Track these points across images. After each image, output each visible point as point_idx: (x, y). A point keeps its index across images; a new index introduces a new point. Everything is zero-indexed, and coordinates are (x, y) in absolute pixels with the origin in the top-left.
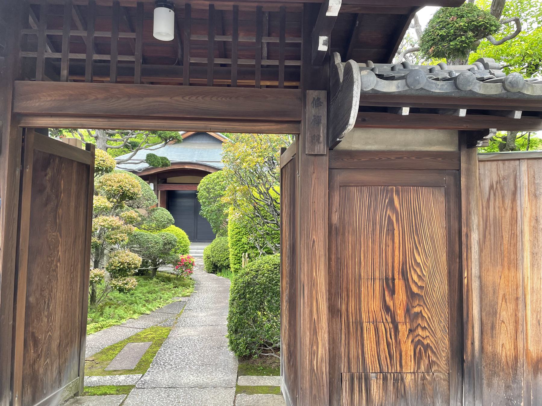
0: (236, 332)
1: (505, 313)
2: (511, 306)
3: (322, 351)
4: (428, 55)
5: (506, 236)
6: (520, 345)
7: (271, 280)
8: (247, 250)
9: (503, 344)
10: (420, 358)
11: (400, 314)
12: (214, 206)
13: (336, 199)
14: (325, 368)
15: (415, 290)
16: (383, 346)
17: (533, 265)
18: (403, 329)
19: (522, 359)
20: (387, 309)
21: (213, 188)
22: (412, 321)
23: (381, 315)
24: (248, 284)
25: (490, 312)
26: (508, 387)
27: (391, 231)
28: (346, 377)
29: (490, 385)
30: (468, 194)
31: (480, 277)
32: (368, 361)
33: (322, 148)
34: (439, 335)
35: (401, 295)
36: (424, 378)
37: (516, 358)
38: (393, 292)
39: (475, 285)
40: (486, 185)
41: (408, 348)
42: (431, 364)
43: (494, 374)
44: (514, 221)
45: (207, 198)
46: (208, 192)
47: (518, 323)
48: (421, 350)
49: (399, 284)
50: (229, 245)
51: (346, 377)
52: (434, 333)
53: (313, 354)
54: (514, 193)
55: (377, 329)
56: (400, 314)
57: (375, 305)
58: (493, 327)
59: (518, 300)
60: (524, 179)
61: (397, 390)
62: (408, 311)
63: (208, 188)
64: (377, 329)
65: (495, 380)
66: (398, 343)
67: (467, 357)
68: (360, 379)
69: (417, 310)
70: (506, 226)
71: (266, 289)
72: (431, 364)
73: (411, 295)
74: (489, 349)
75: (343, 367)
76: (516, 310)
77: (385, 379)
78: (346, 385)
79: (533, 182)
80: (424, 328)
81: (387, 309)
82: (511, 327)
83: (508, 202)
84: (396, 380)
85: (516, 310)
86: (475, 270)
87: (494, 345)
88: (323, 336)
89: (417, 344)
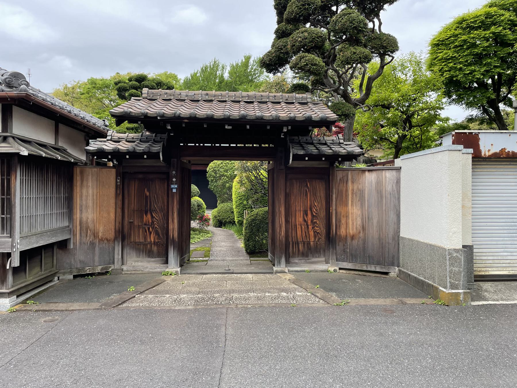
0: (248, 241)
1: (343, 221)
2: (345, 219)
3: (283, 233)
4: (233, 256)
5: (344, 195)
6: (348, 231)
7: (263, 218)
8: (243, 208)
9: (342, 231)
10: (316, 237)
11: (309, 222)
12: (220, 183)
13: (288, 184)
14: (284, 239)
15: (314, 214)
16: (304, 232)
17: (351, 205)
18: (310, 227)
19: (348, 236)
20: (305, 220)
21: (219, 170)
22: (313, 225)
23: (302, 222)
24: (253, 220)
25: (338, 221)
26: (344, 245)
27: (306, 195)
28: (291, 243)
29: (338, 245)
30: (332, 182)
31: (336, 210)
32: (298, 236)
33: (283, 167)
34: (322, 229)
35: (310, 216)
36: (317, 243)
37: (346, 236)
38: (307, 215)
39: (334, 212)
40: (339, 178)
41: (312, 233)
42: (319, 238)
43: (340, 241)
44: (347, 190)
45: (214, 177)
46: (216, 173)
47: (347, 224)
48: (316, 234)
49: (309, 212)
50: (234, 207)
51: (291, 243)
52: (320, 229)
53: (280, 235)
54: (347, 182)
55: (301, 227)
56: (309, 222)
57: (301, 220)
58: (340, 226)
59: (347, 217)
60: (350, 177)
61: (308, 247)
62: (312, 221)
63: (214, 170)
64: (301, 227)
65: (340, 243)
66: (308, 232)
67: (331, 236)
68: (296, 244)
69: (315, 221)
70: (344, 193)
71: (261, 221)
72: (319, 238)
73: (313, 216)
74: (338, 233)
75: (290, 240)
76: (347, 220)
77: (304, 244)
78: (291, 246)
79: (352, 178)
80: (317, 227)
81: (305, 220)
82: (345, 226)
83: (345, 184)
84: (308, 244)
85: (347, 220)
86: (334, 207)
87: (340, 232)
88: (283, 229)
89: (314, 232)
